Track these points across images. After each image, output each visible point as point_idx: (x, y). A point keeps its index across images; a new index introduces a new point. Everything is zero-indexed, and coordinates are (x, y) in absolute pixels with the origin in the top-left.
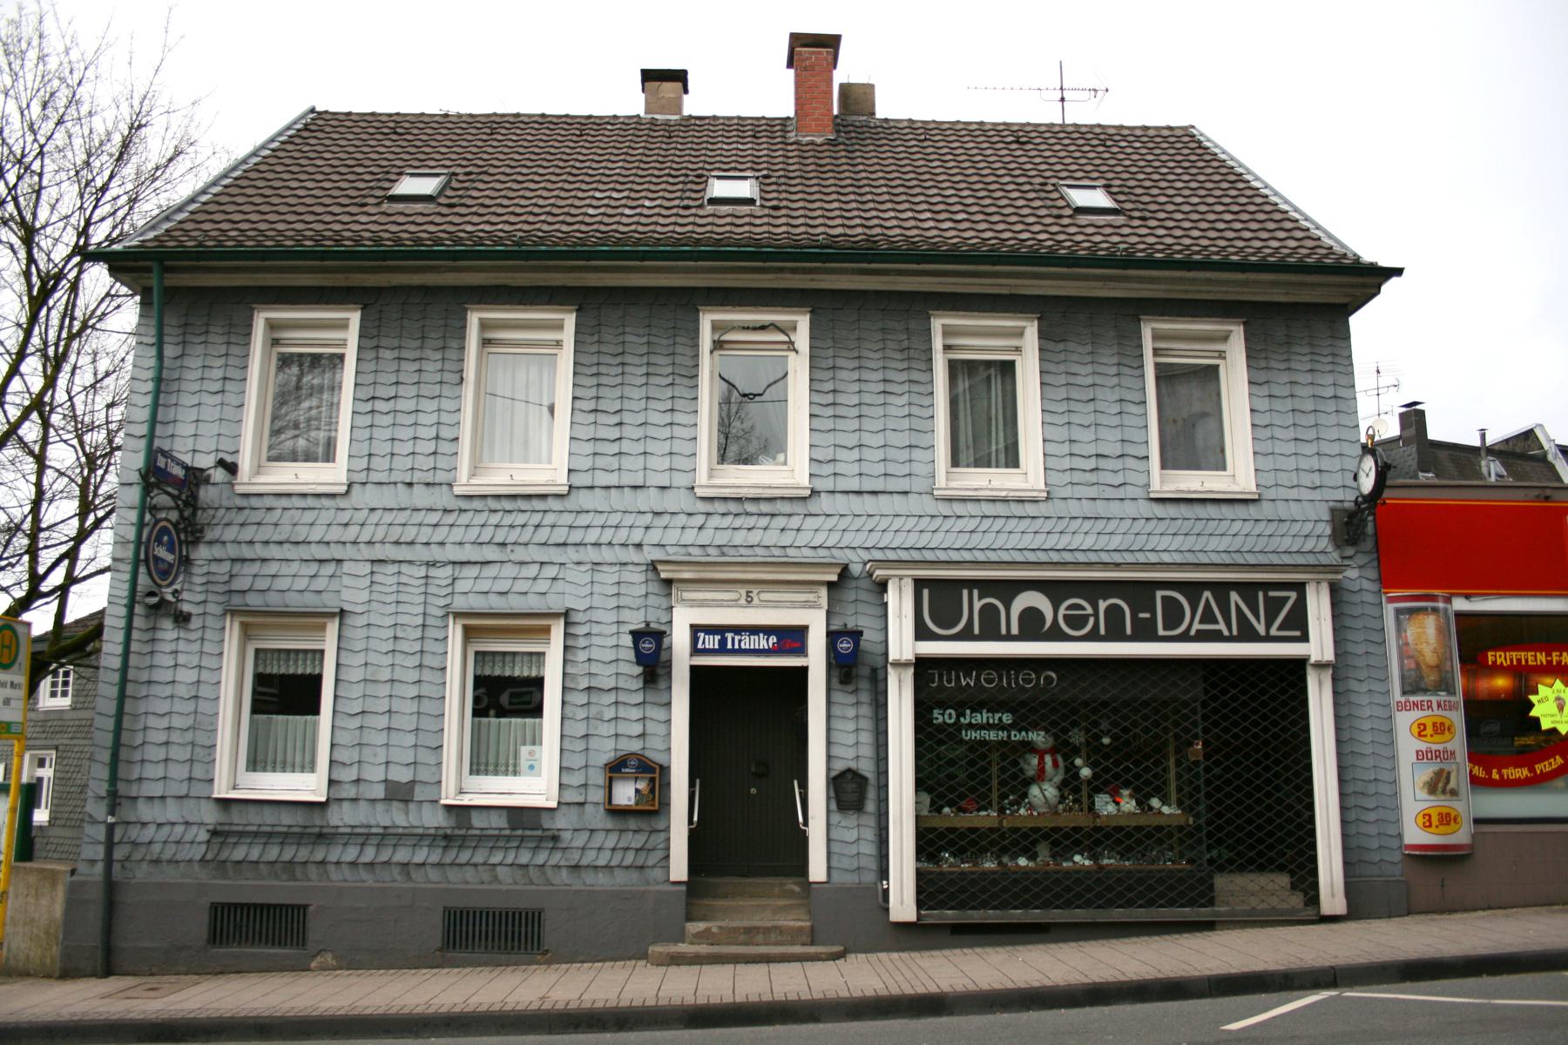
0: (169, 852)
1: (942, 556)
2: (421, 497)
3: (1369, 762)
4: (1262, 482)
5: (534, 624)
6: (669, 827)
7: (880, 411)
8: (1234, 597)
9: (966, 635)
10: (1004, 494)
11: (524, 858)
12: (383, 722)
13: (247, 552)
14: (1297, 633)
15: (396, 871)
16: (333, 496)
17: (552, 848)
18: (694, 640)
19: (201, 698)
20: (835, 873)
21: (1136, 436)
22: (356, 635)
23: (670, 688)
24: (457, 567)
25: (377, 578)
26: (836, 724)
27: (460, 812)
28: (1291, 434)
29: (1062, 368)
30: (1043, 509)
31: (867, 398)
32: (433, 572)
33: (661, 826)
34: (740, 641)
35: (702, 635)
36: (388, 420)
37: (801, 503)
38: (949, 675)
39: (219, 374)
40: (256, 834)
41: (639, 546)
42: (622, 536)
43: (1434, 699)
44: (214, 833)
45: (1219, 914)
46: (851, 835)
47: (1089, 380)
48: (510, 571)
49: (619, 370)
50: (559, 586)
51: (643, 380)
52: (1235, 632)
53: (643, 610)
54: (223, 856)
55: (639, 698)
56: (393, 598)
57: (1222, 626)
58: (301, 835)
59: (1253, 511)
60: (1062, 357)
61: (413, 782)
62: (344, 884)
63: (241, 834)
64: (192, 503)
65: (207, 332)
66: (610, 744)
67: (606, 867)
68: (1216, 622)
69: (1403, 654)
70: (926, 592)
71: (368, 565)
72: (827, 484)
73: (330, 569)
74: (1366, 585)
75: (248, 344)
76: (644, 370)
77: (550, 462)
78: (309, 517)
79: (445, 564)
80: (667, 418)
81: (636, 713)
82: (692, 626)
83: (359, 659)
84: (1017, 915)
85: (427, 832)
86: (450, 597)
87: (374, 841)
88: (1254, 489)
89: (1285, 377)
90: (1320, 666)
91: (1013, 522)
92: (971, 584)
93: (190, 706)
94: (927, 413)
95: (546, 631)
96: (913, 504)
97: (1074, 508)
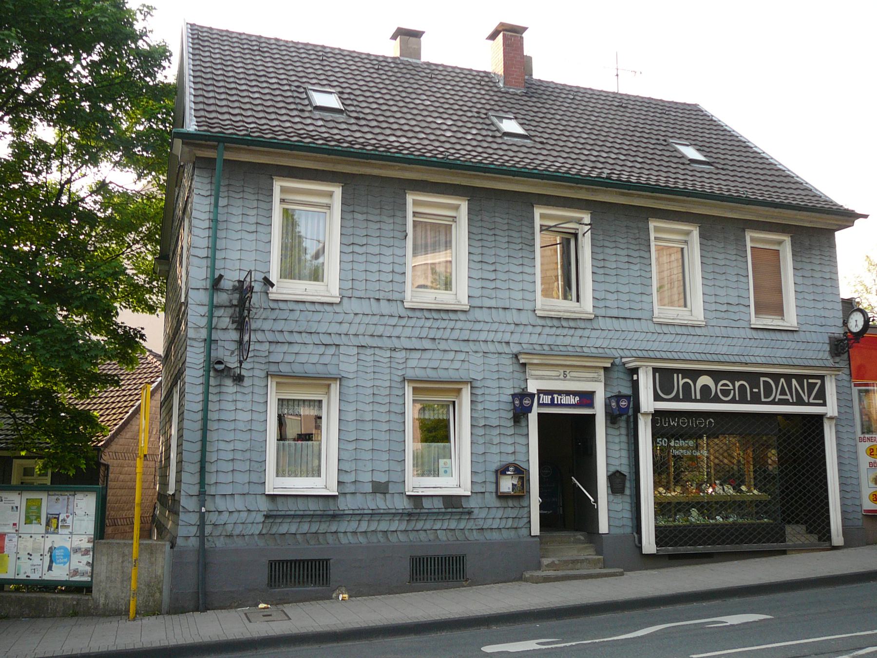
0: (237, 531)
1: (658, 355)
5: (454, 387)
7: (626, 273)
8: (794, 382)
9: (676, 399)
10: (686, 322)
12: (368, 445)
14: (821, 402)
15: (380, 535)
16: (332, 304)
19: (256, 431)
24: (408, 351)
27: (417, 499)
32: (394, 354)
33: (525, 504)
35: (542, 395)
36: (362, 258)
37: (589, 322)
39: (253, 220)
41: (508, 343)
42: (499, 336)
44: (267, 517)
45: (789, 546)
48: (438, 355)
51: (506, 245)
52: (795, 401)
54: (273, 531)
55: (511, 431)
56: (372, 369)
57: (789, 397)
61: (388, 482)
62: (430, 543)
66: (497, 458)
70: (657, 374)
71: (356, 348)
72: (602, 312)
73: (332, 350)
76: (506, 239)
77: (323, 281)
78: (318, 316)
80: (519, 269)
83: (352, 407)
85: (397, 511)
86: (404, 370)
88: (796, 325)
89: (809, 267)
90: (831, 418)
93: (246, 436)
95: (459, 391)
96: (644, 325)
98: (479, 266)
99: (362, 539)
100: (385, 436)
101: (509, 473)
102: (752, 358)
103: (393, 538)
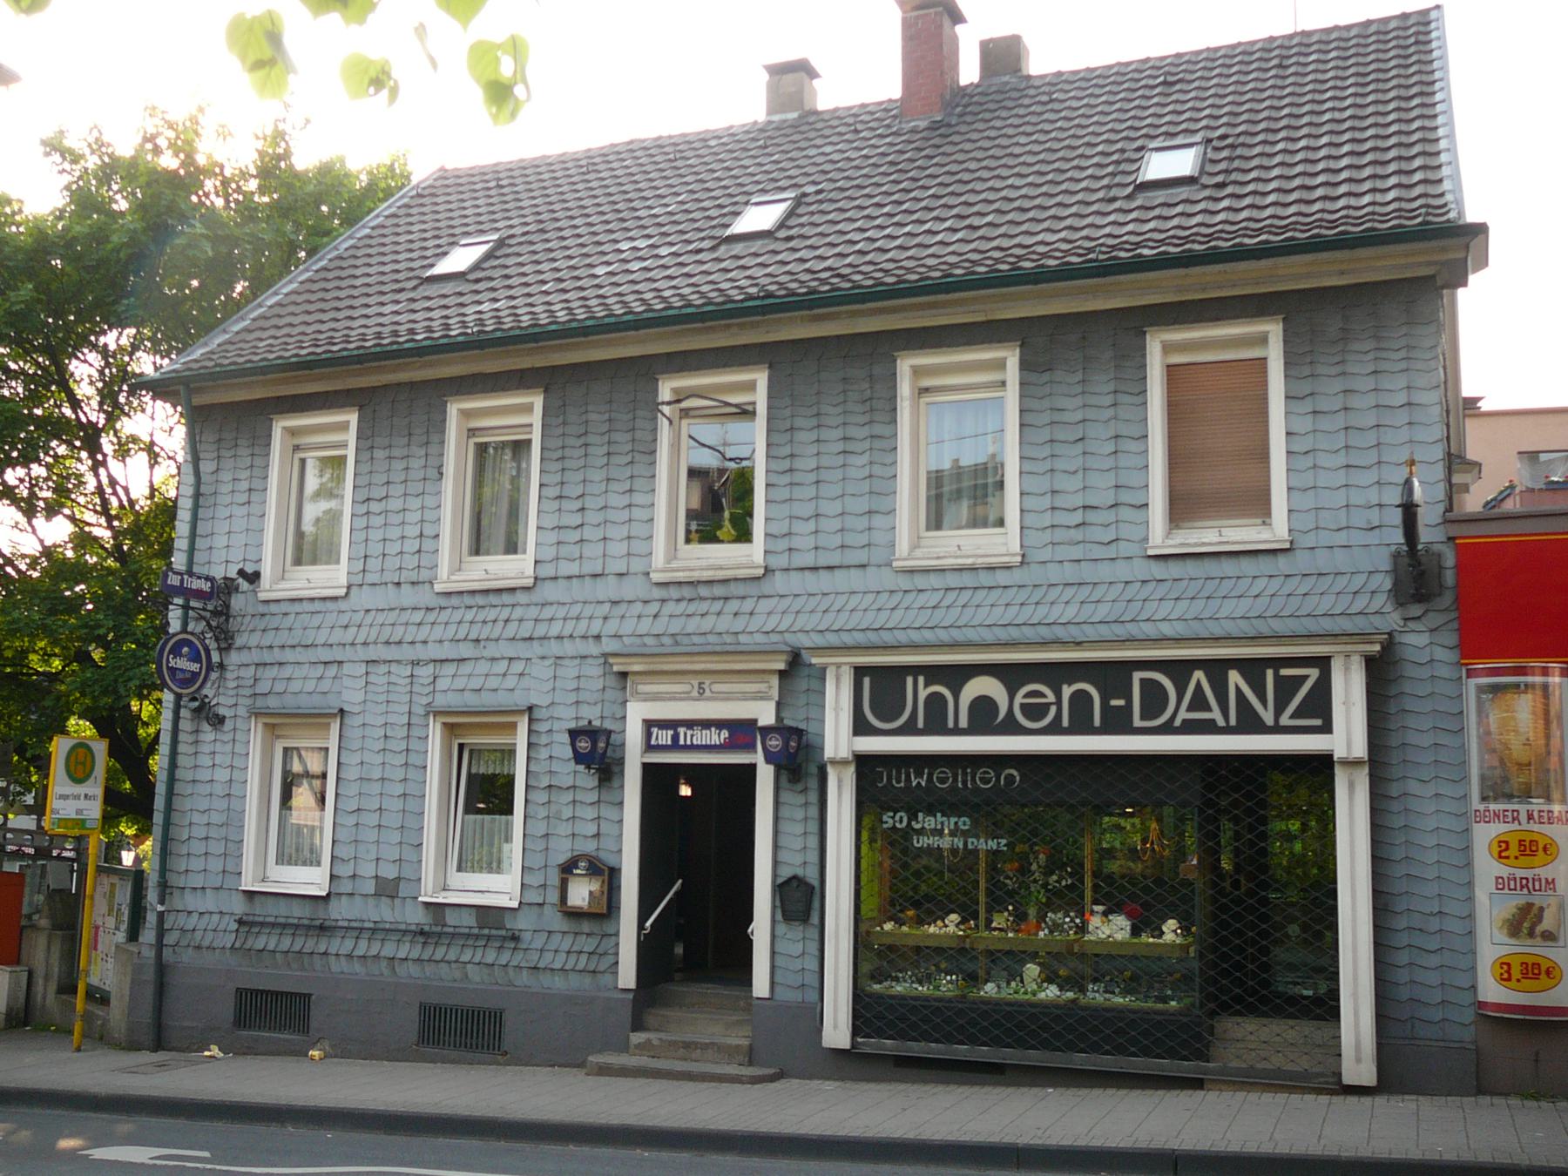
2: (408, 596)
3: (1432, 889)
4: (1297, 526)
6: (618, 931)
7: (838, 474)
8: (1234, 677)
9: (909, 729)
10: (969, 561)
11: (490, 956)
12: (373, 819)
13: (267, 657)
14: (1318, 722)
15: (384, 964)
16: (335, 599)
17: (515, 949)
18: (648, 735)
19: (232, 794)
20: (778, 989)
21: (1134, 479)
22: (353, 734)
23: (622, 786)
24: (438, 664)
25: (372, 678)
26: (784, 826)
28: (1341, 459)
29: (1046, 403)
30: (1017, 577)
31: (825, 461)
32: (419, 671)
34: (692, 736)
35: (655, 730)
38: (899, 773)
39: (244, 485)
40: (273, 925)
41: (598, 637)
42: (582, 627)
43: (1523, 809)
46: (797, 949)
47: (1079, 416)
48: (483, 667)
49: (582, 452)
50: (526, 681)
52: (1233, 722)
53: (600, 705)
55: (593, 797)
57: (1216, 714)
58: (309, 927)
59: (1282, 563)
60: (1047, 390)
61: (399, 879)
63: (262, 924)
64: (224, 612)
65: (236, 445)
67: (562, 969)
68: (1209, 709)
69: (1486, 746)
70: (867, 681)
73: (332, 670)
74: (1440, 654)
75: (268, 455)
76: (605, 449)
78: (316, 620)
79: (427, 663)
80: (625, 500)
81: (590, 813)
82: (645, 721)
83: (356, 759)
84: (962, 1051)
87: (366, 935)
90: (1354, 763)
91: (981, 594)
92: (916, 670)
94: (888, 472)
95: (513, 726)
96: (872, 579)
97: (1054, 574)
98: (556, 504)
99: (357, 967)
100: (397, 804)
101: (578, 871)
102: (1210, 624)
103: (401, 970)
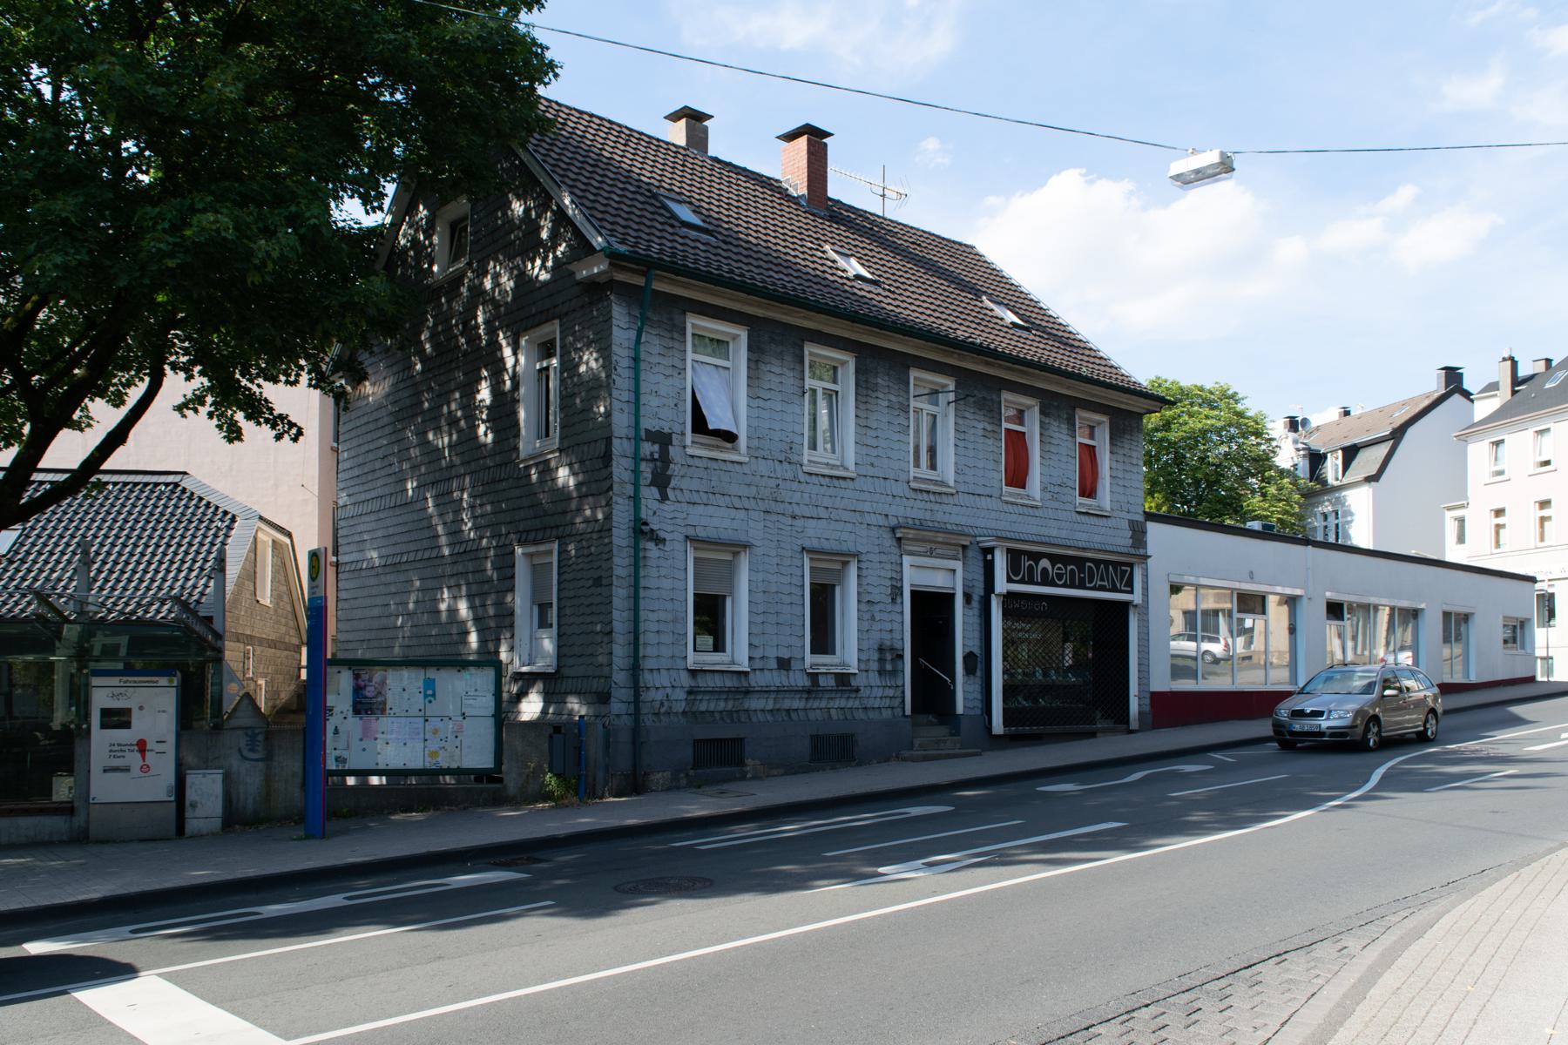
5: (844, 558)
15: (784, 713)
44: (690, 693)
